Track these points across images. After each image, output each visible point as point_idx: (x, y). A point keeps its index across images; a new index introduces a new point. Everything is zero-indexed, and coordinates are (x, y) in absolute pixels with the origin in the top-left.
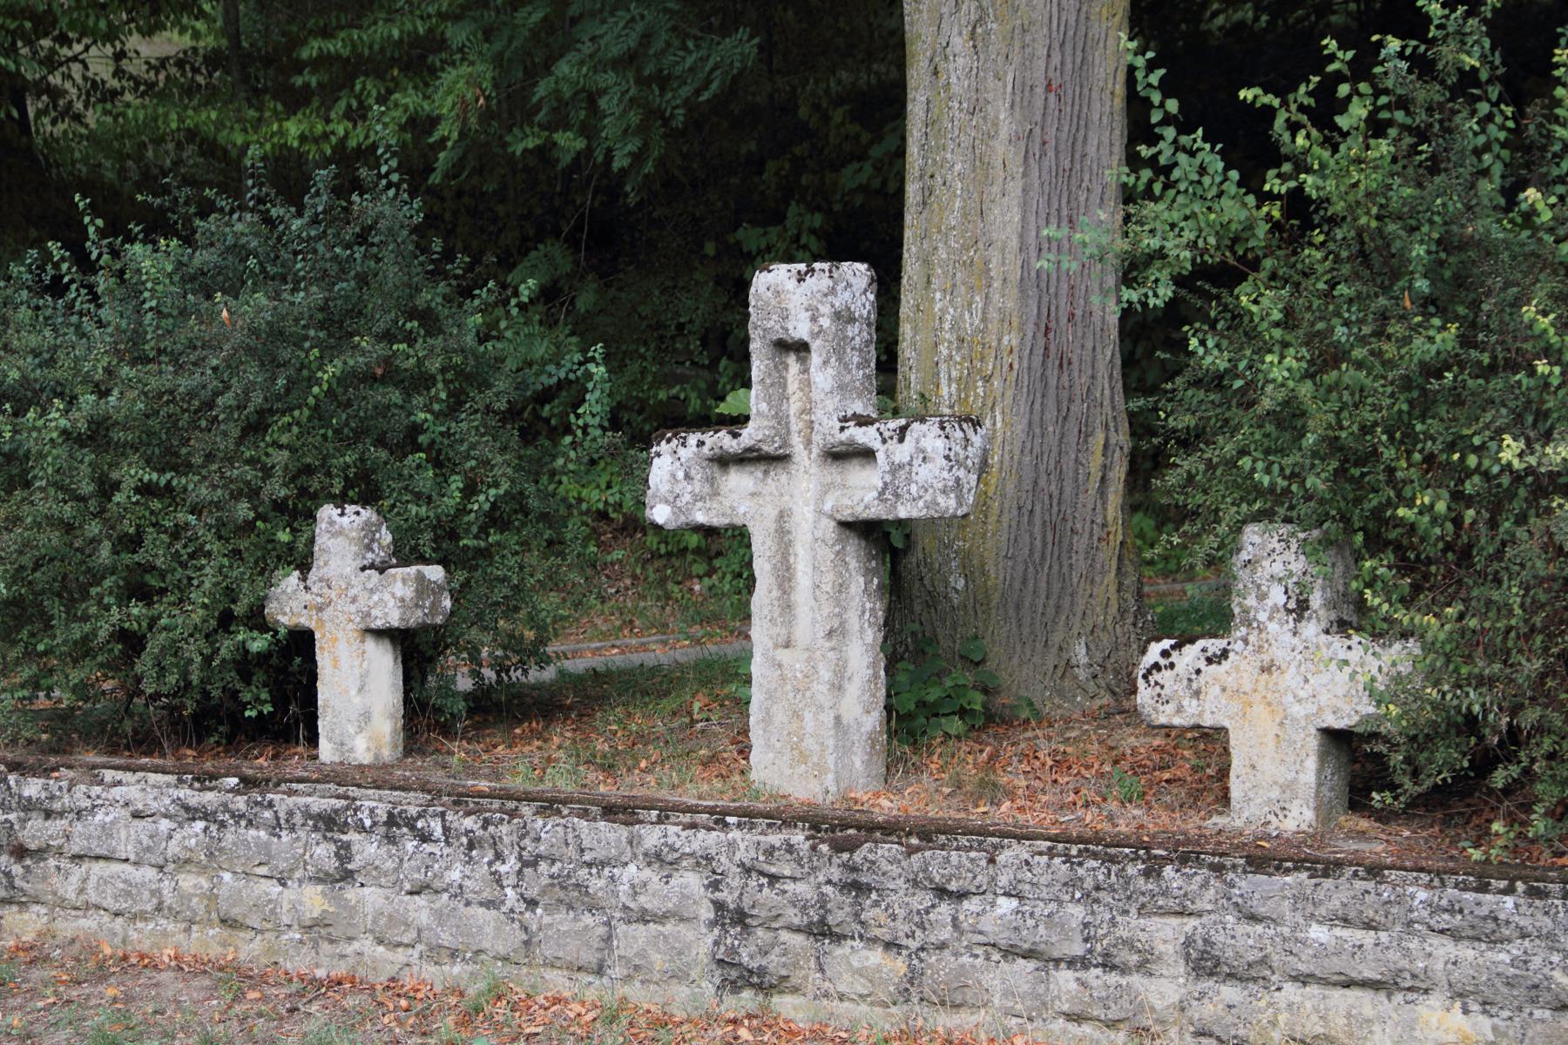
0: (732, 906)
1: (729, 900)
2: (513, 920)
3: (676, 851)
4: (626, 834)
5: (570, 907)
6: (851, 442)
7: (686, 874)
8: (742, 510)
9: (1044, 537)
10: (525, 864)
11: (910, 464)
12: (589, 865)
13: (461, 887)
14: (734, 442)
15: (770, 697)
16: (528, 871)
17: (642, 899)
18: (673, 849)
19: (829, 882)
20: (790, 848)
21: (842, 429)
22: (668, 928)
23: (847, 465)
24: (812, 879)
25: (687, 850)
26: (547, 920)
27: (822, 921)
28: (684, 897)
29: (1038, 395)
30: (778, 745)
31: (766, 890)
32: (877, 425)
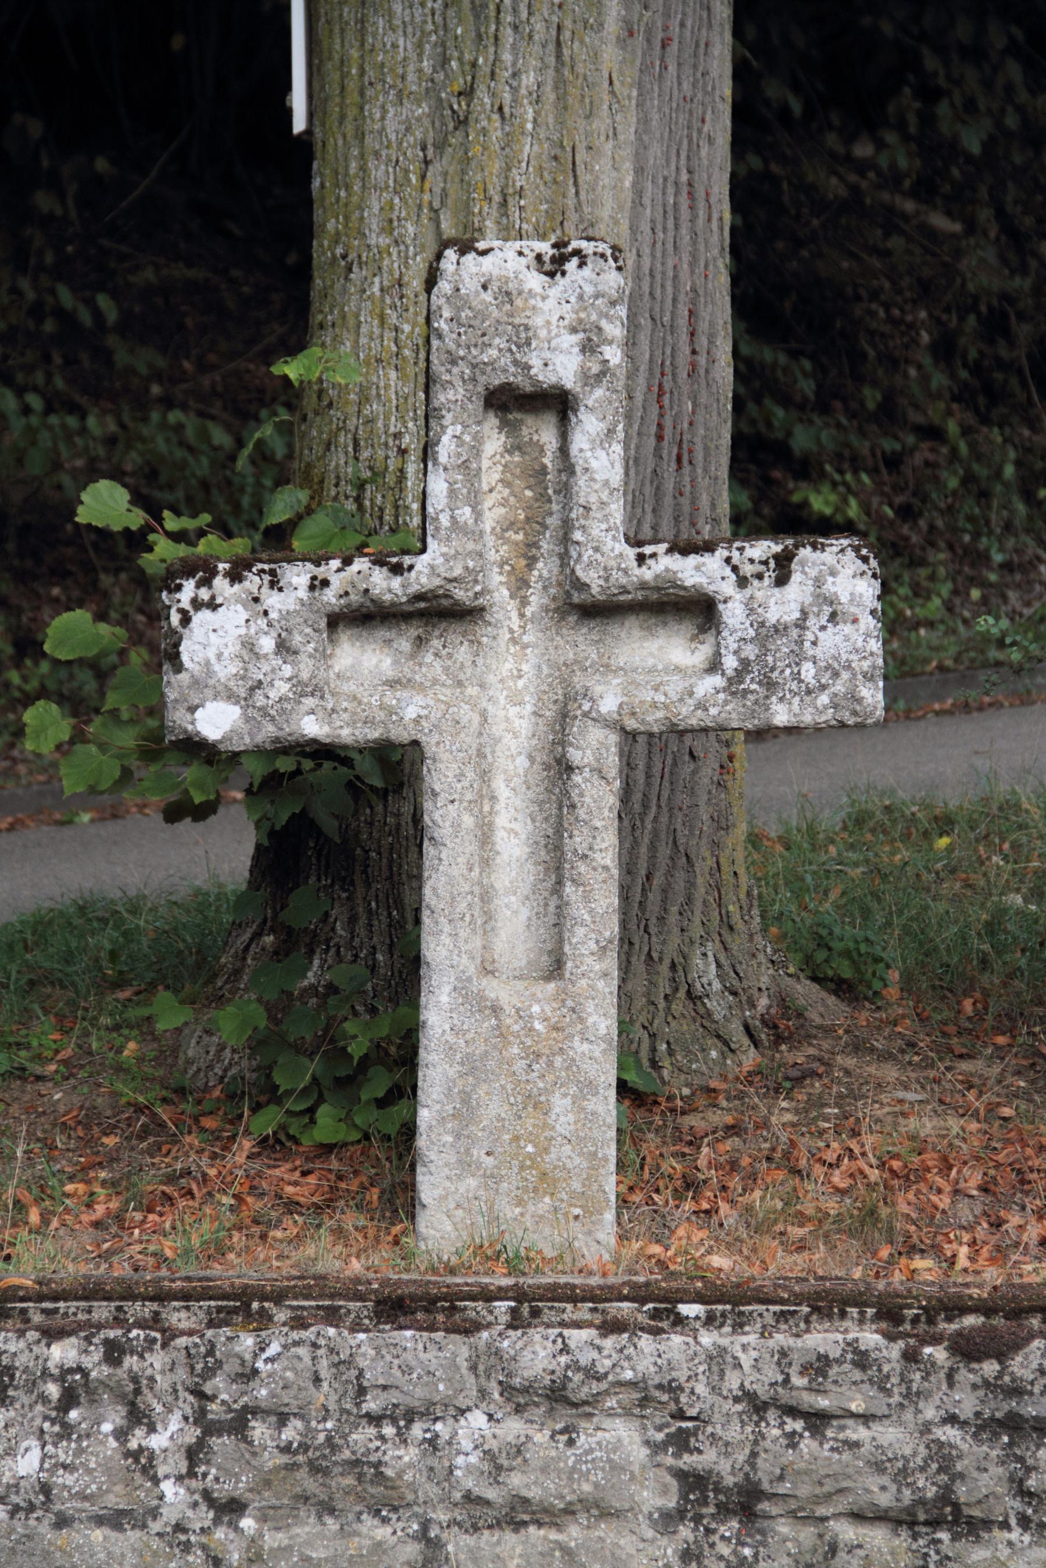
0: (729, 1481)
1: (724, 1467)
2: (187, 1547)
3: (599, 1378)
4: (464, 1352)
5: (327, 1508)
6: (670, 582)
7: (607, 1423)
8: (410, 713)
9: (649, 767)
10: (210, 1429)
11: (801, 624)
12: (375, 1419)
13: (46, 1489)
14: (396, 582)
15: (472, 1071)
16: (221, 1443)
17: (516, 1480)
18: (591, 1373)
19: (952, 1419)
20: (862, 1360)
21: (641, 559)
22: (574, 1534)
23: (614, 628)
24: (908, 1415)
25: (629, 1375)
26: (272, 1540)
27: (946, 1496)
28: (616, 1468)
29: (648, 509)
30: (489, 1161)
31: (807, 1444)
32: (721, 553)
